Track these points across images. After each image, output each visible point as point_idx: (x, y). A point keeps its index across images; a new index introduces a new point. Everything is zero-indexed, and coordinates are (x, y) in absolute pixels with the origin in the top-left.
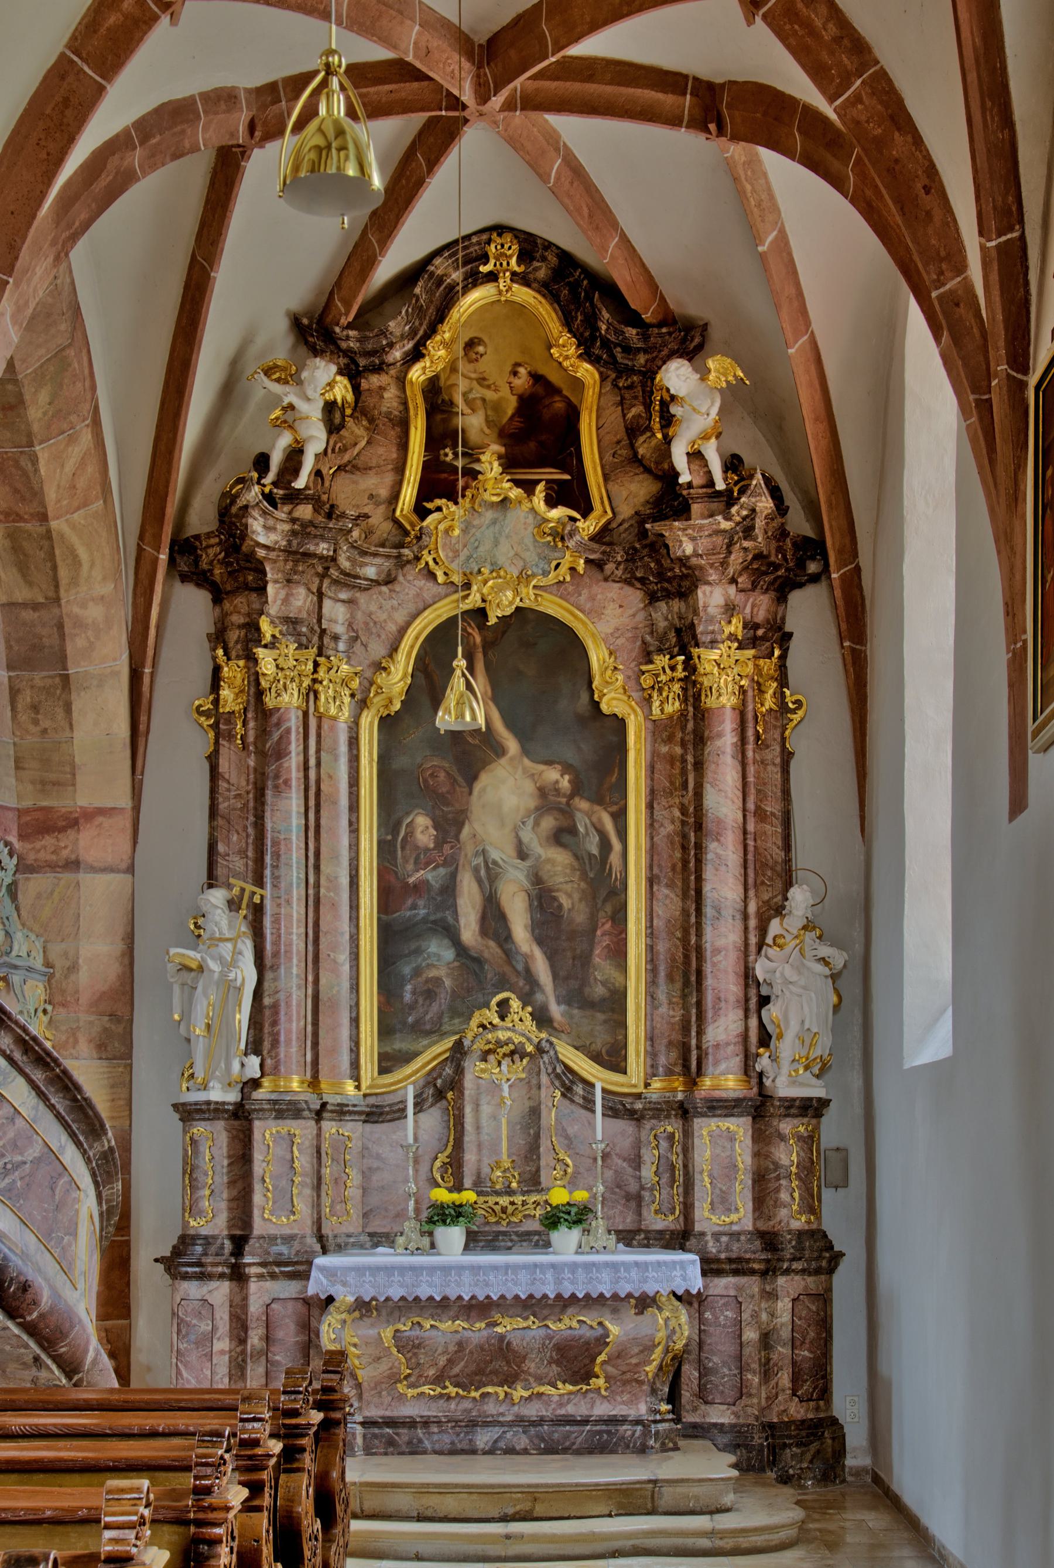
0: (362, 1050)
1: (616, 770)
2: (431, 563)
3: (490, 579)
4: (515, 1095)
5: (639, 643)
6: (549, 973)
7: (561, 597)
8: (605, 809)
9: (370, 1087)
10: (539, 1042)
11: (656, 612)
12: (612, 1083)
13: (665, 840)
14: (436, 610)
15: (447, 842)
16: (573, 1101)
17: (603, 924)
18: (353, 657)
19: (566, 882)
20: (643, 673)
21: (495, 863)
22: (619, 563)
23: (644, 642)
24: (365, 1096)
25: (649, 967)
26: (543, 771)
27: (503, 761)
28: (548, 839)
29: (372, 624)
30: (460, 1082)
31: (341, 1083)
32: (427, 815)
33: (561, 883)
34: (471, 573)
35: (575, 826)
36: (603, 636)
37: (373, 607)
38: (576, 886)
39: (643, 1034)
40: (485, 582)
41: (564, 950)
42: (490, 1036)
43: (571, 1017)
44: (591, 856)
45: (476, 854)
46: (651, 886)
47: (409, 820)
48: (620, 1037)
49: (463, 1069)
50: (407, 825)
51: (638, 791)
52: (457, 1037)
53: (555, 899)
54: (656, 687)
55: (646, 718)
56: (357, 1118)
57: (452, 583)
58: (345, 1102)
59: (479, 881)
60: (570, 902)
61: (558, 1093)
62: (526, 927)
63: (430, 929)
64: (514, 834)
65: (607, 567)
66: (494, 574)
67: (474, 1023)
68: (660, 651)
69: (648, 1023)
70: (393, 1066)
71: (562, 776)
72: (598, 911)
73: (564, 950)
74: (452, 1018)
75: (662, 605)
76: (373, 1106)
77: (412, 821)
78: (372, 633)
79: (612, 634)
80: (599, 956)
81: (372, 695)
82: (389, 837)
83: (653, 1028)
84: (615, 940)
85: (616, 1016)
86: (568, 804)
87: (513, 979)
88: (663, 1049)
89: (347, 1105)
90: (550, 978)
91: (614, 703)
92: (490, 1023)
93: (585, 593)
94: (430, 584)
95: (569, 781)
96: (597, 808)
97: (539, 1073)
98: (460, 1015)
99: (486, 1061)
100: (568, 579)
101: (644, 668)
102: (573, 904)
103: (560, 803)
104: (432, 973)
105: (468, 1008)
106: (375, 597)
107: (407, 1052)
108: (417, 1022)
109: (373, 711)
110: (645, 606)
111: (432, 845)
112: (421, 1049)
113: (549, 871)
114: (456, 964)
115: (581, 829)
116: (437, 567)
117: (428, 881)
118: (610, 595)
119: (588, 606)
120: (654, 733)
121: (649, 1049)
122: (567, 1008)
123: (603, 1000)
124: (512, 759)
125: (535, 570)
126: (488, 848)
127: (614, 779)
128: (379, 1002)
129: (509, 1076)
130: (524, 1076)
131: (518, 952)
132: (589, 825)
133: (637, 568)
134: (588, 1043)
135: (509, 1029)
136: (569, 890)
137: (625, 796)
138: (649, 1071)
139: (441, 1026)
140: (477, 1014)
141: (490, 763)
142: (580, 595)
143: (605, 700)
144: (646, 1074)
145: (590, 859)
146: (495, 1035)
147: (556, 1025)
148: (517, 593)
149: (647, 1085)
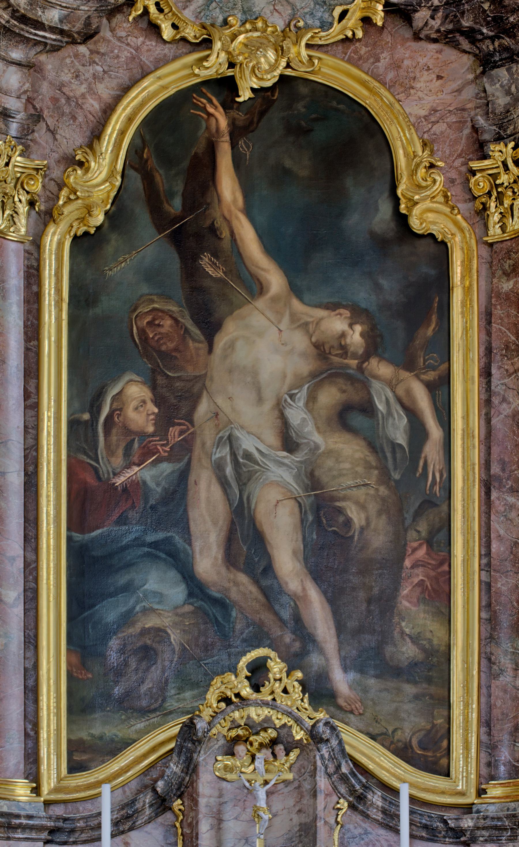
0: (43, 735)
1: (434, 318)
2: (153, 9)
3: (240, 33)
4: (277, 806)
5: (467, 131)
6: (331, 624)
7: (349, 61)
8: (417, 376)
9: (56, 790)
10: (314, 726)
11: (493, 84)
12: (427, 790)
13: (510, 421)
14: (159, 78)
15: (174, 425)
16: (367, 816)
17: (414, 550)
18: (34, 147)
19: (357, 486)
20: (473, 173)
21: (248, 456)
22: (436, 10)
23: (475, 129)
24: (47, 804)
25: (484, 615)
26: (321, 319)
27: (261, 303)
28: (329, 421)
29: (63, 101)
30: (192, 783)
31: (8, 783)
32: (144, 383)
33: (350, 488)
34: (213, 25)
35: (370, 402)
36: (413, 119)
37: (66, 77)
38: (372, 492)
39: (475, 715)
40: (234, 37)
41: (354, 589)
42: (237, 715)
43: (365, 690)
44: (395, 446)
45: (219, 443)
46: (488, 493)
47: (115, 391)
48: (439, 721)
49: (196, 766)
50: (114, 398)
51: (467, 350)
52: (184, 719)
53: (340, 511)
54: (495, 194)
55: (480, 241)
56: (34, 835)
57: (184, 39)
58: (16, 811)
59: (224, 483)
60: (363, 516)
61: (344, 804)
62: (295, 553)
63: (148, 555)
64: (276, 412)
65: (417, 15)
66: (248, 26)
67: (212, 696)
68: (499, 139)
69: (483, 700)
70: (91, 760)
71: (351, 326)
72: (406, 530)
73: (354, 589)
74: (181, 690)
75: (502, 73)
76: (58, 818)
77: (120, 393)
78: (63, 114)
79: (425, 117)
80: (407, 598)
81: (61, 202)
82: (86, 416)
83: (490, 707)
84: (432, 573)
85: (433, 690)
86: (360, 369)
87: (276, 631)
88: (506, 738)
89: (18, 816)
90: (333, 631)
91: (431, 216)
92: (237, 695)
93: (385, 58)
94: (152, 43)
95: (362, 335)
96: (404, 374)
97: (313, 774)
98: (195, 685)
99: (233, 754)
100: (360, 34)
101: (475, 165)
102: (367, 519)
103: (348, 367)
104: (152, 622)
105: (206, 674)
106: (68, 61)
107: (112, 741)
108: (127, 694)
109: (63, 226)
110: (476, 78)
111: (151, 429)
112: (135, 736)
113: (330, 470)
114: (188, 608)
115: (381, 407)
116: (162, 16)
117: (144, 483)
118: (423, 61)
119: (390, 76)
120: (491, 263)
121: (484, 738)
122: (358, 676)
123: (414, 664)
124: (275, 300)
125: (310, 22)
126: (237, 433)
127: (430, 332)
128: (69, 663)
129: (267, 777)
130: (290, 776)
131: (281, 591)
132: (392, 400)
133: (463, 13)
134: (390, 729)
135: (266, 704)
136: (362, 499)
137: (448, 358)
138: (484, 771)
139: (164, 701)
140: (217, 681)
141: (240, 307)
142: (378, 60)
143: (416, 211)
144: (479, 776)
145: (394, 452)
146: (245, 714)
147: (341, 702)
148: (280, 51)
149: (481, 792)
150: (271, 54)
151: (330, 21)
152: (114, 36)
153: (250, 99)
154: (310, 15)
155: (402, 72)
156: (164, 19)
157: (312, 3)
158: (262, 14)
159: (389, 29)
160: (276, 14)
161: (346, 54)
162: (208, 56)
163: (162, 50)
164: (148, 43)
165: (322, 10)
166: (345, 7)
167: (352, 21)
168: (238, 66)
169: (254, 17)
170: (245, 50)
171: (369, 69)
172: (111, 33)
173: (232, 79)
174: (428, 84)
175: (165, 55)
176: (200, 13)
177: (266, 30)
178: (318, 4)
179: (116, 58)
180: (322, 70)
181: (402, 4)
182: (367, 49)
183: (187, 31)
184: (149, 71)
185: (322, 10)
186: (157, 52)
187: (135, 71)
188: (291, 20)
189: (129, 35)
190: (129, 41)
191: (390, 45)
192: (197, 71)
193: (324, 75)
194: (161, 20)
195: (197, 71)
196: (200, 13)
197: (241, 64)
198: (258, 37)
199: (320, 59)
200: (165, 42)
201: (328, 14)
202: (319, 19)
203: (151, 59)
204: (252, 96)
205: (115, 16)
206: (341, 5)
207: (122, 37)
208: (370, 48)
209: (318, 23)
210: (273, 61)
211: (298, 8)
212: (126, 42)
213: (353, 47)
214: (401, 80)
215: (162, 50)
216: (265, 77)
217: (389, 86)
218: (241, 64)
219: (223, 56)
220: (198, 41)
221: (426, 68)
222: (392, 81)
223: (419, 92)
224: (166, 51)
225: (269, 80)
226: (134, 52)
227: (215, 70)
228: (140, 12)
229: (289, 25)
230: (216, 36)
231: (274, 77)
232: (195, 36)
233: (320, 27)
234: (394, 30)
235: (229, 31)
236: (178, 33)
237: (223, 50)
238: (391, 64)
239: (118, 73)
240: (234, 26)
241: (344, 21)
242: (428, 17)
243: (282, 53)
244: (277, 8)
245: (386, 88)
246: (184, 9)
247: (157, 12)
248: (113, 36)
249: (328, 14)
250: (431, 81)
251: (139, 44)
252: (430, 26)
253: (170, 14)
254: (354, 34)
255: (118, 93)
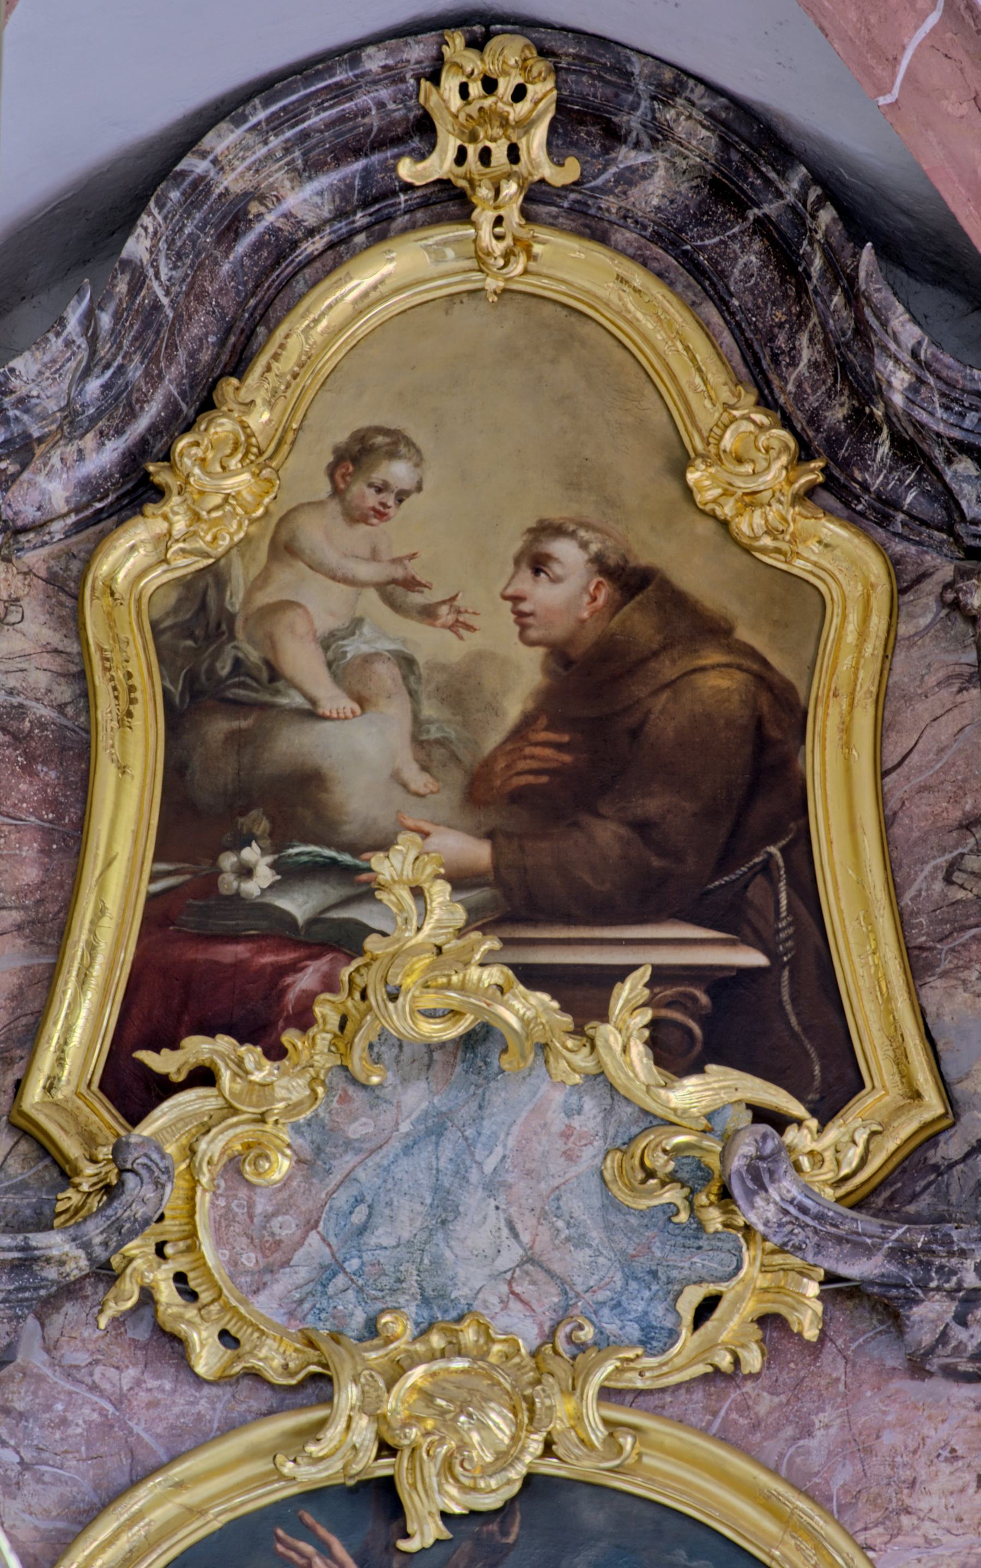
2: (167, 1293)
14: (180, 1486)
34: (336, 1337)
40: (393, 1378)
57: (254, 1375)
65: (917, 1312)
66: (436, 1340)
100: (753, 1360)
116: (191, 1312)
118: (936, 1434)
119: (843, 1476)
125: (612, 1328)
142: (807, 1431)
150: (498, 1420)
151: (668, 1324)
152: (55, 1363)
153: (438, 1541)
154: (613, 1308)
155: (877, 1467)
156: (198, 1320)
157: (618, 1277)
158: (477, 1305)
159: (840, 1342)
160: (515, 1305)
161: (715, 1414)
162: (322, 1424)
163: (192, 1403)
164: (152, 1383)
165: (647, 1294)
166: (712, 1288)
167: (733, 1324)
168: (407, 1453)
169: (454, 1314)
170: (421, 1411)
171: (781, 1456)
172: (45, 1357)
173: (387, 1486)
174: (952, 1500)
175: (199, 1417)
176: (301, 1302)
177: (488, 1352)
178: (636, 1279)
179: (58, 1426)
180: (646, 1460)
181: (872, 1283)
182: (776, 1400)
183: (263, 1353)
184: (152, 1462)
185: (647, 1294)
186: (176, 1410)
187: (111, 1463)
188: (559, 1323)
189: (97, 1362)
190: (97, 1377)
191: (841, 1387)
192: (288, 1468)
193: (652, 1476)
194: (190, 1323)
195: (288, 1468)
196: (301, 1302)
197: (413, 1450)
198: (463, 1371)
199: (635, 1429)
200: (199, 1381)
201: (664, 1305)
202: (637, 1320)
203: (159, 1430)
204: (446, 1534)
205: (58, 1309)
206: (700, 1281)
207: (77, 1367)
208: (783, 1398)
209: (634, 1331)
210: (506, 1441)
211: (579, 1289)
212: (88, 1380)
213: (734, 1395)
214: (875, 1490)
215: (192, 1403)
216: (482, 1484)
217: (840, 1506)
218: (413, 1450)
219: (364, 1431)
220: (293, 1382)
221: (946, 1453)
222: (847, 1492)
223: (927, 1525)
224: (203, 1406)
225: (493, 1491)
226: (110, 1409)
227: (339, 1465)
228: (129, 1304)
229: (551, 1337)
230: (343, 1372)
231: (509, 1482)
232: (286, 1367)
233: (642, 1343)
234: (853, 1346)
235: (382, 1352)
236: (239, 1357)
237: (362, 1410)
238: (844, 1442)
239: (61, 1468)
240: (397, 1338)
241: (709, 1325)
242: (949, 1317)
243: (531, 1420)
244: (518, 1289)
245: (831, 1513)
246: (256, 1292)
247: (178, 1299)
248: (52, 1365)
249: (664, 1305)
250: (962, 1490)
251: (125, 1388)
252: (953, 1343)
253: (215, 1308)
254: (737, 1362)
255: (61, 1525)
